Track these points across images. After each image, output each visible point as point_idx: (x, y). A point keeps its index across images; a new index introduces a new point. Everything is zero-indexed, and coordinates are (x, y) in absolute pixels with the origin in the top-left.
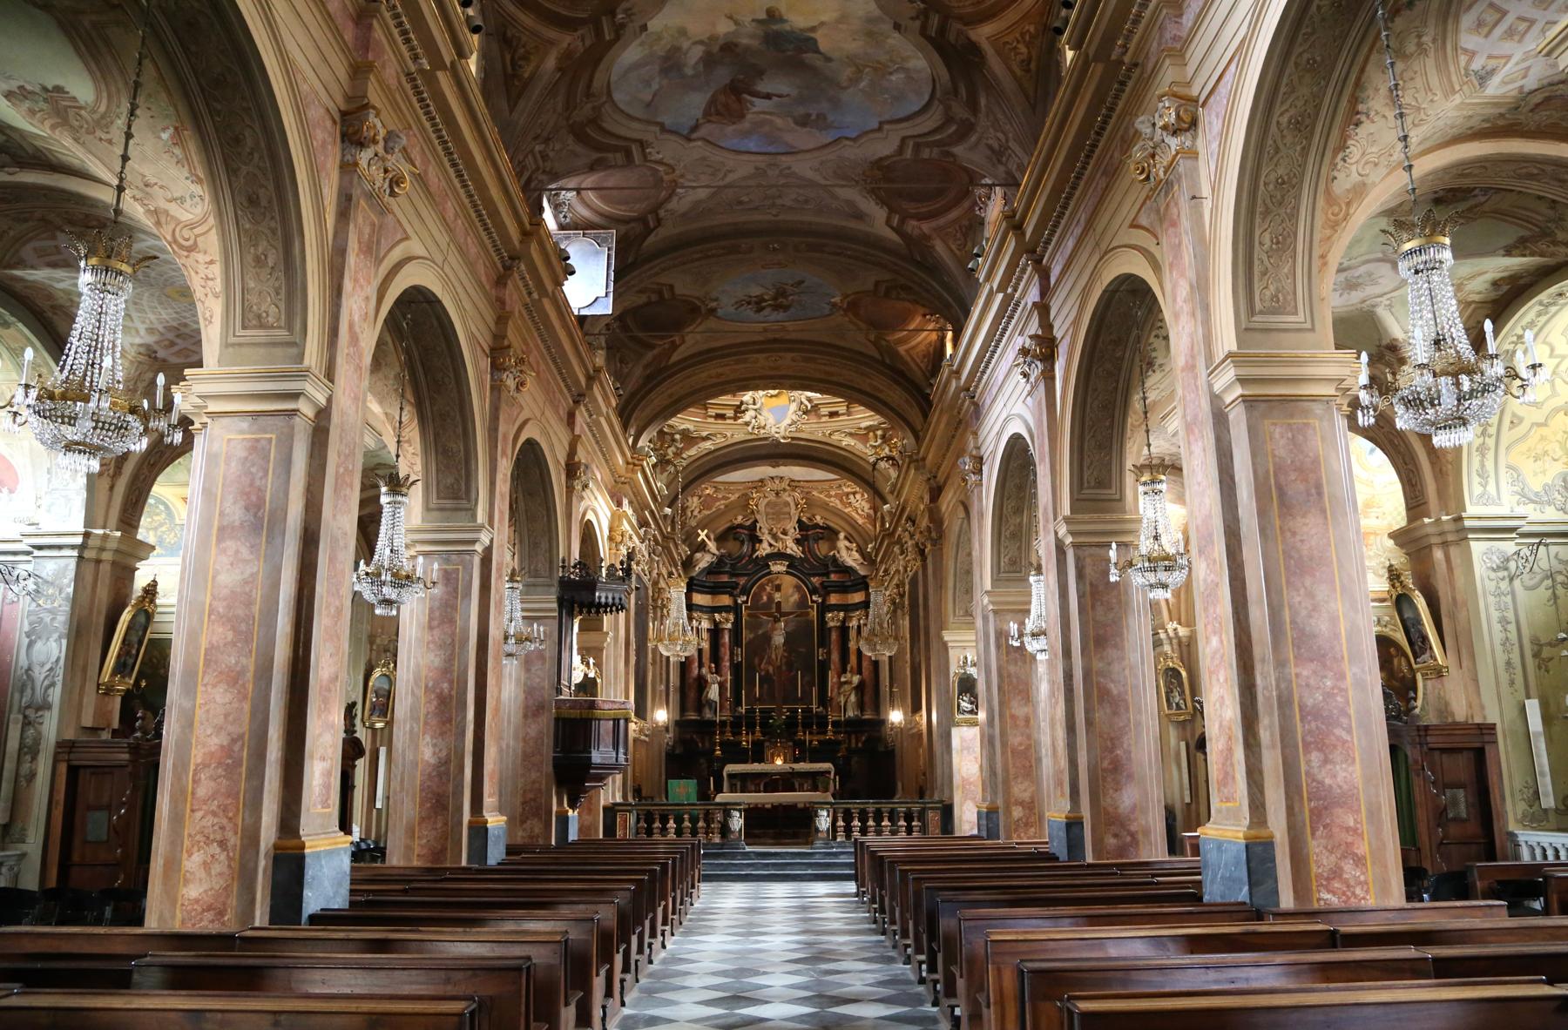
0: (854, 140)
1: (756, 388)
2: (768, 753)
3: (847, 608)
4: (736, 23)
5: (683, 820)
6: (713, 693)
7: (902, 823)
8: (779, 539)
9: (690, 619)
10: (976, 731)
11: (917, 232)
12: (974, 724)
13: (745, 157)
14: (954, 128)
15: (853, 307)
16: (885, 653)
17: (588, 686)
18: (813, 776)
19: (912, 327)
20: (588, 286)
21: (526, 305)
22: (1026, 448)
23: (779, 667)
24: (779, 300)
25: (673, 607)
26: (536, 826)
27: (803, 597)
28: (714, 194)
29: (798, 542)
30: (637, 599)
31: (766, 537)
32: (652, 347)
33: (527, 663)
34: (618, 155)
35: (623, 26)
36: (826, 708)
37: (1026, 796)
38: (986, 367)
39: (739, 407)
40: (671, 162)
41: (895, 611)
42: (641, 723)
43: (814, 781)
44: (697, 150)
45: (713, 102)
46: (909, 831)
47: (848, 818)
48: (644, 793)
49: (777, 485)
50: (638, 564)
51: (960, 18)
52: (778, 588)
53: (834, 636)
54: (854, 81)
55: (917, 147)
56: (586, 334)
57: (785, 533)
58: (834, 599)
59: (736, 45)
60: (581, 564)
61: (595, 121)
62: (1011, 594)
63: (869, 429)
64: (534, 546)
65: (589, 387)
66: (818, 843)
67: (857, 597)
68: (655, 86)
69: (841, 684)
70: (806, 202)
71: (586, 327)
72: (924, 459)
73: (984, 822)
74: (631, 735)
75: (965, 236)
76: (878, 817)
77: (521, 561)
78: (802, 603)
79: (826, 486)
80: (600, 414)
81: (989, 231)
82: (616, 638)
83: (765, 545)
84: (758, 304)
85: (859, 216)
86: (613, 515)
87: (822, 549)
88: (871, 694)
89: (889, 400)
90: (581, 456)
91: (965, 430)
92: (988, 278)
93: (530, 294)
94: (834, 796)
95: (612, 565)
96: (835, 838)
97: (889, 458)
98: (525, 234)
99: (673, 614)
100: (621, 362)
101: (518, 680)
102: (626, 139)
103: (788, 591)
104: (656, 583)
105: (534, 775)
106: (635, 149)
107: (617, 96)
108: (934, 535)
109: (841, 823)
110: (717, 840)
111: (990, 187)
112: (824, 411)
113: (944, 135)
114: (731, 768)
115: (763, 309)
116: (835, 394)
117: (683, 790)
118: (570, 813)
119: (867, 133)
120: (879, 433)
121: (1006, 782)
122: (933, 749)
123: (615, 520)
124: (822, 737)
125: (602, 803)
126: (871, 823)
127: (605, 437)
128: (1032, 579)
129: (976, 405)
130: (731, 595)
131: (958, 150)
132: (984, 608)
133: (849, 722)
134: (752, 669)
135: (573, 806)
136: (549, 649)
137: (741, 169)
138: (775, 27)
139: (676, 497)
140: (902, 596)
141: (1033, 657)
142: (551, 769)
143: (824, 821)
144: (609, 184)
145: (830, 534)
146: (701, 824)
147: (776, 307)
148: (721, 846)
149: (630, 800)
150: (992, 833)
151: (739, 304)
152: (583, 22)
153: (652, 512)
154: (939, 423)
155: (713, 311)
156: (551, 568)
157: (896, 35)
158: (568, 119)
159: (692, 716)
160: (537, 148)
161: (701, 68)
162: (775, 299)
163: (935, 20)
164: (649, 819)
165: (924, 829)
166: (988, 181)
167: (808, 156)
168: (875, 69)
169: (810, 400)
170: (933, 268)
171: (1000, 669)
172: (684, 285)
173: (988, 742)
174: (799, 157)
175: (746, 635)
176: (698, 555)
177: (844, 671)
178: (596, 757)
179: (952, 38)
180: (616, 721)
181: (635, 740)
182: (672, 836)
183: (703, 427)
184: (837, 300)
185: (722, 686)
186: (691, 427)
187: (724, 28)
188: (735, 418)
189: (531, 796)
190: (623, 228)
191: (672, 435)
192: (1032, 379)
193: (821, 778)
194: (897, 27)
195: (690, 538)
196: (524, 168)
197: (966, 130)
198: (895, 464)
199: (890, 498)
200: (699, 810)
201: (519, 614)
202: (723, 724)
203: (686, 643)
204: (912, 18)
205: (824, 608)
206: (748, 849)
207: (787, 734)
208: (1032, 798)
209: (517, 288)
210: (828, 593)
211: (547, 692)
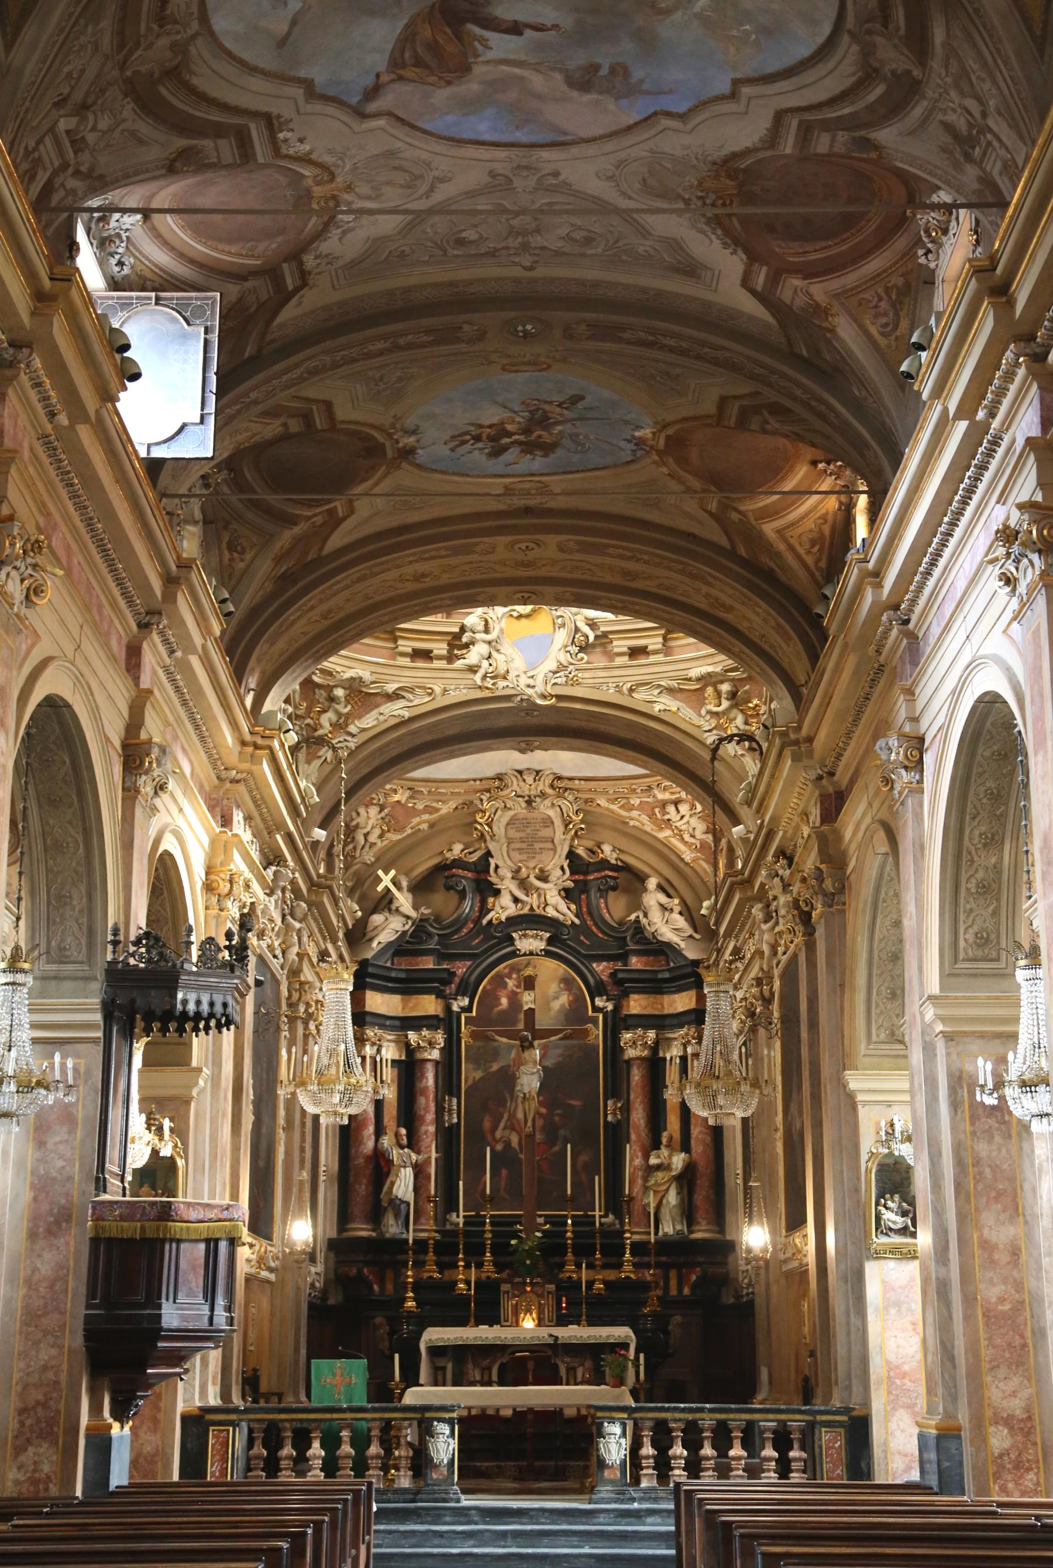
0: (682, 117)
1: (491, 601)
2: (508, 1305)
3: (662, 1022)
5: (338, 1442)
6: (403, 1185)
7: (769, 1452)
8: (533, 887)
9: (360, 1040)
10: (912, 1268)
11: (801, 301)
12: (911, 1255)
13: (470, 151)
14: (879, 90)
15: (676, 446)
16: (735, 1114)
17: (159, 1173)
18: (595, 1351)
19: (788, 486)
20: (168, 398)
21: (44, 437)
22: (1008, 722)
23: (531, 1136)
24: (536, 433)
25: (327, 1019)
26: (44, 1457)
27: (578, 1003)
28: (410, 227)
29: (568, 894)
30: (259, 1004)
31: (508, 885)
32: (291, 521)
33: (40, 1130)
34: (223, 143)
36: (619, 1216)
37: (1016, 1406)
38: (933, 564)
39: (457, 636)
40: (327, 159)
41: (753, 1029)
42: (261, 1245)
43: (596, 1362)
44: (377, 136)
45: (407, 38)
46: (784, 1468)
47: (662, 1439)
48: (264, 1387)
49: (528, 786)
50: (261, 935)
52: (529, 983)
53: (637, 1075)
55: (806, 132)
56: (164, 495)
57: (543, 877)
58: (636, 1005)
60: (150, 938)
61: (176, 72)
62: (977, 1004)
63: (707, 680)
64: (58, 901)
65: (170, 597)
66: (605, 1491)
67: (682, 1002)
69: (650, 1170)
70: (588, 241)
71: (164, 479)
72: (810, 740)
73: (933, 1456)
74: (242, 1269)
75: (896, 306)
76: (722, 1439)
77: (32, 930)
78: (576, 1014)
79: (623, 787)
80: (190, 649)
81: (943, 298)
82: (216, 1080)
83: (505, 900)
84: (496, 441)
85: (690, 269)
86: (213, 842)
87: (614, 908)
88: (706, 1189)
89: (743, 626)
90: (153, 729)
91: (891, 684)
92: (940, 389)
93: (52, 415)
94: (634, 1393)
95: (210, 940)
96: (636, 1481)
97: (743, 737)
98: (41, 298)
99: (328, 1031)
100: (231, 547)
101: (20, 1164)
102: (237, 111)
103: (548, 990)
104: (294, 973)
105: (46, 1353)
106: (256, 131)
107: (220, 23)
108: (828, 885)
109: (648, 1450)
110: (405, 1481)
111: (949, 209)
112: (620, 645)
113: (861, 105)
114: (435, 1335)
115: (504, 449)
116: (637, 614)
117: (341, 1380)
118: (116, 1429)
120: (725, 687)
121: (975, 1376)
122: (828, 1305)
123: (219, 850)
124: (611, 1275)
125: (180, 1407)
126: (707, 1451)
127: (199, 692)
128: (1021, 975)
129: (912, 637)
130: (440, 995)
131: (885, 135)
132: (926, 1028)
133: (666, 1246)
134: (478, 1139)
135: (120, 1415)
136: (83, 1103)
137: (463, 175)
139: (334, 810)
140: (767, 1001)
141: (1025, 1127)
142: (79, 1341)
143: (614, 1446)
144: (201, 202)
145: (630, 880)
146: (374, 1449)
147: (529, 448)
148: (414, 1495)
149: (237, 1401)
150: (949, 1479)
151: (459, 439)
153: (289, 838)
154: (840, 672)
155: (408, 453)
156: (91, 945)
158: (122, 66)
159: (362, 1231)
160: (63, 125)
162: (527, 431)
164: (272, 1438)
165: (812, 1467)
166: (944, 196)
167: (591, 150)
169: (592, 624)
170: (831, 370)
171: (958, 1148)
172: (352, 404)
173: (937, 1292)
174: (575, 151)
175: (468, 1074)
176: (377, 919)
177: (656, 1145)
178: (171, 1316)
180: (212, 1244)
181: (249, 1279)
182: (316, 1474)
183: (391, 675)
184: (646, 433)
185: (419, 1171)
186: (366, 675)
188: (451, 658)
189: (38, 1395)
190: (234, 290)
191: (330, 689)
192: (1022, 588)
193: (609, 1358)
195: (361, 885)
196: (38, 162)
197: (904, 93)
198: (755, 748)
199: (744, 812)
200: (372, 1420)
201: (24, 1035)
202: (421, 1245)
203: (349, 1094)
205: (617, 1023)
206: (466, 1501)
207: (546, 1267)
208: (1028, 1409)
209: (26, 402)
210: (626, 994)
211: (79, 1188)
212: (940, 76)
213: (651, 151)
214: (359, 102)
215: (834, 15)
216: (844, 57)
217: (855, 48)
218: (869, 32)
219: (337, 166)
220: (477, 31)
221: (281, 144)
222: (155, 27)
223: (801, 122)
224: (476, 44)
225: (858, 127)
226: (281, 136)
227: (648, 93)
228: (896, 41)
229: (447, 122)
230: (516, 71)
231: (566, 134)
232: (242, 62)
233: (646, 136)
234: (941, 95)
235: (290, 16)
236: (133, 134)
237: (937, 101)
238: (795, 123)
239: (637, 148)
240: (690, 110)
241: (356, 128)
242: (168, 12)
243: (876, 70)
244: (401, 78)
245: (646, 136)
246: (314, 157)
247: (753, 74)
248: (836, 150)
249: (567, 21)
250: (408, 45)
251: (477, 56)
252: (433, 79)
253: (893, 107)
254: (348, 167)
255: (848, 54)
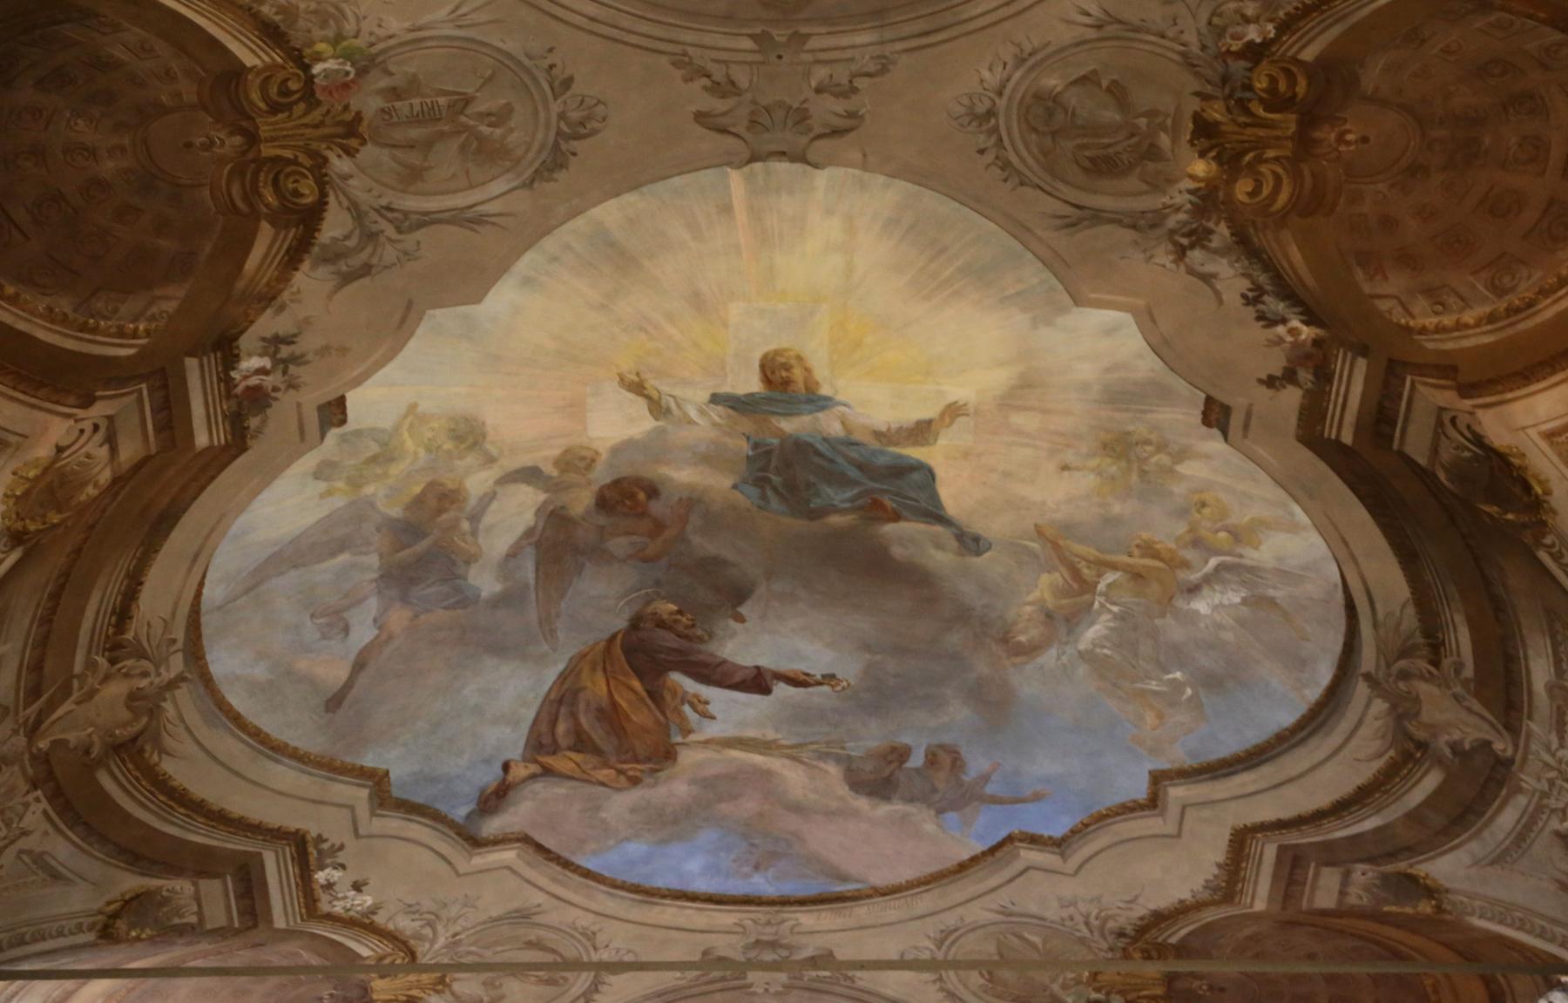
0: (1059, 845)
4: (657, 408)
13: (670, 913)
14: (1431, 781)
34: (213, 890)
35: (258, 399)
40: (405, 925)
44: (499, 882)
45: (564, 697)
51: (1446, 370)
54: (1063, 620)
55: (1293, 866)
59: (653, 491)
61: (133, 750)
68: (363, 634)
106: (275, 867)
107: (224, 661)
119: (1102, 819)
131: (1447, 868)
138: (789, 426)
152: (112, 375)
157: (1214, 444)
158: (33, 730)
161: (527, 569)
163: (1353, 384)
167: (891, 910)
168: (1137, 576)
174: (863, 912)
179: (1416, 441)
187: (614, 424)
194: (1216, 415)
197: (1478, 785)
204: (1270, 382)
212: (1548, 748)
213: (1003, 911)
214: (469, 816)
215: (1338, 648)
216: (1360, 722)
217: (1379, 706)
218: (1405, 675)
219: (419, 937)
220: (689, 685)
221: (319, 892)
222: (102, 661)
223: (1282, 849)
224: (687, 709)
225: (1392, 855)
226: (321, 876)
227: (995, 800)
228: (1458, 689)
229: (625, 856)
230: (757, 759)
231: (844, 878)
232: (257, 734)
233: (993, 882)
234: (1551, 783)
235: (352, 657)
236: (40, 860)
237: (1544, 795)
238: (1270, 852)
239: (976, 907)
240: (1073, 832)
241: (462, 866)
242: (130, 636)
243: (1422, 746)
244: (547, 772)
245: (993, 882)
246: (380, 919)
247: (1189, 762)
248: (1352, 900)
249: (850, 669)
250: (563, 710)
251: (687, 732)
252: (604, 774)
253: (1459, 813)
254: (441, 941)
255: (1367, 714)
